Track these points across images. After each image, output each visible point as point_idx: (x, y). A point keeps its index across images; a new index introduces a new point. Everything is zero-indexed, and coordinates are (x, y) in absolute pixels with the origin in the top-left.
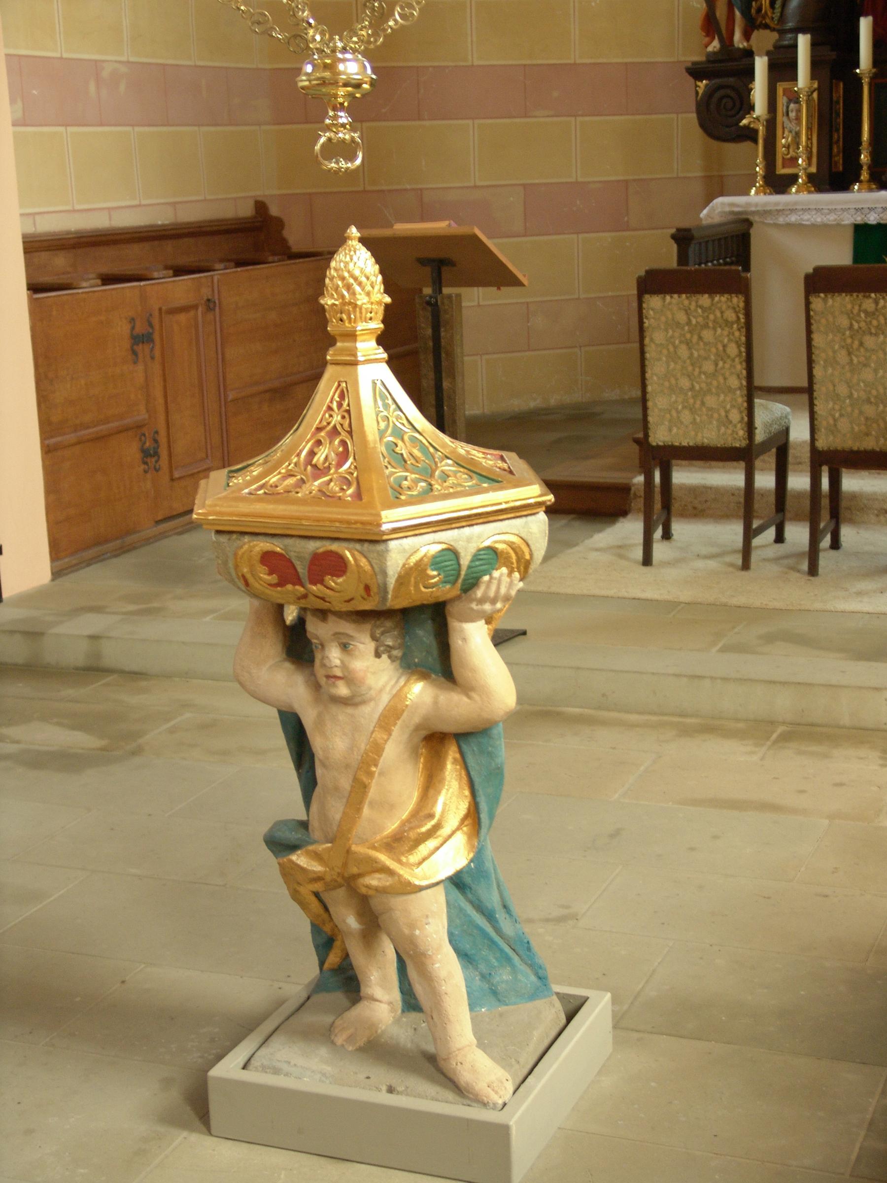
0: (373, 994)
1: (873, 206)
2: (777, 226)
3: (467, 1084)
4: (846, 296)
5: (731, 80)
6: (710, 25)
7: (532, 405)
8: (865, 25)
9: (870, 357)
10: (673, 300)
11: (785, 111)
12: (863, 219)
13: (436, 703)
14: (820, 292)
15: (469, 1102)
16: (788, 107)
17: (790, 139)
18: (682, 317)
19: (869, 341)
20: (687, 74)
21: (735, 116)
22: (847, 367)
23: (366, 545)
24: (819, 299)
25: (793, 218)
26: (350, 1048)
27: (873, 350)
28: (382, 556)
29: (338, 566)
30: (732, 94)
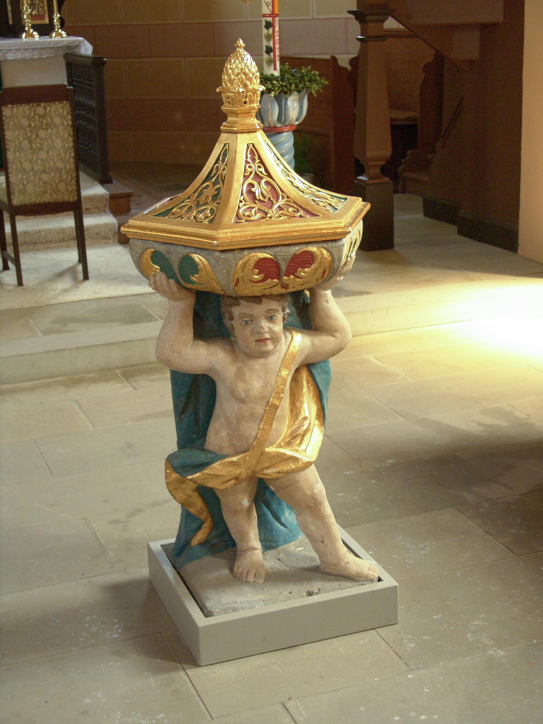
0: (254, 546)
3: (357, 573)
4: (26, 105)
9: (43, 143)
13: (313, 344)
14: (8, 104)
15: (362, 583)
19: (42, 134)
22: (29, 151)
23: (330, 244)
24: (8, 108)
26: (261, 582)
27: (45, 139)
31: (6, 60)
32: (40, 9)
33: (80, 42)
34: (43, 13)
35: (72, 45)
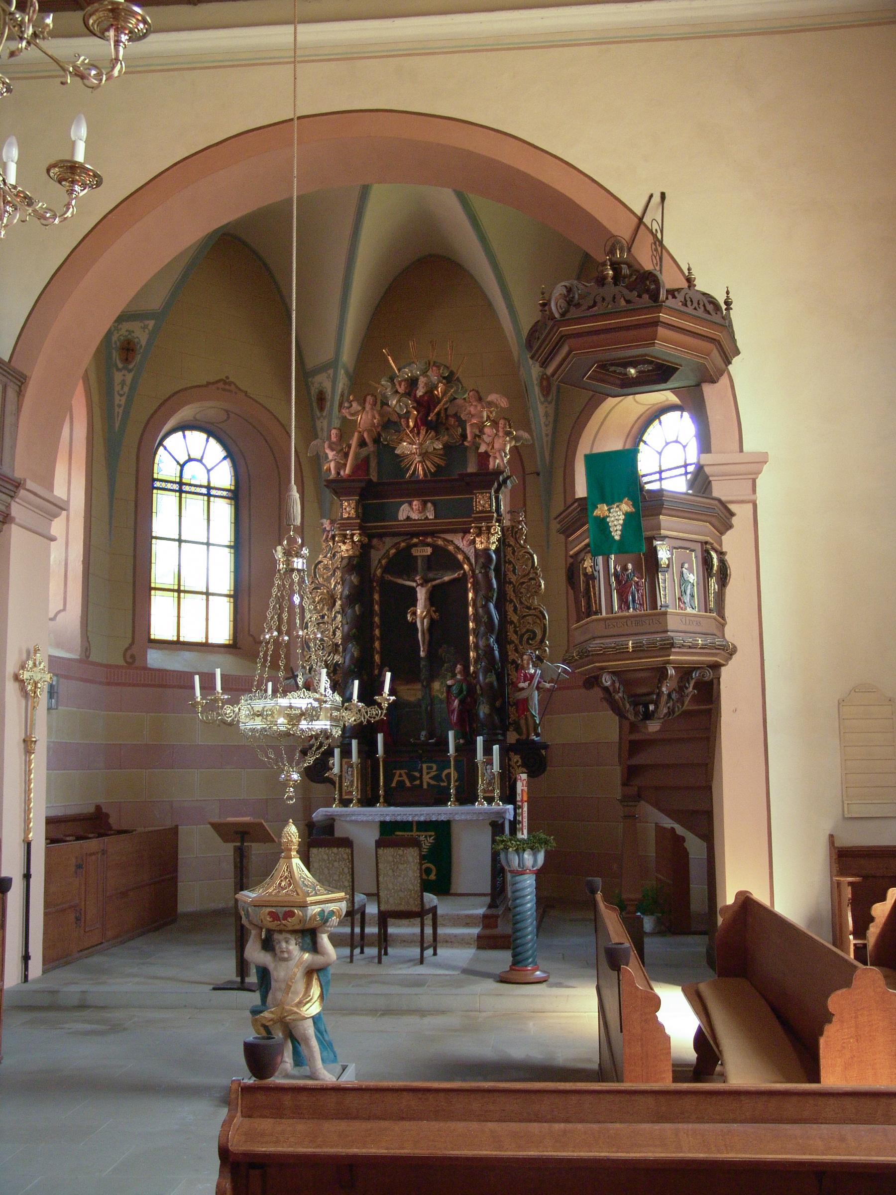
2: (346, 821)
7: (221, 906)
8: (380, 737)
10: (322, 850)
18: (326, 857)
19: (401, 867)
25: (353, 818)
28: (306, 911)
29: (292, 914)
31: (454, 820)
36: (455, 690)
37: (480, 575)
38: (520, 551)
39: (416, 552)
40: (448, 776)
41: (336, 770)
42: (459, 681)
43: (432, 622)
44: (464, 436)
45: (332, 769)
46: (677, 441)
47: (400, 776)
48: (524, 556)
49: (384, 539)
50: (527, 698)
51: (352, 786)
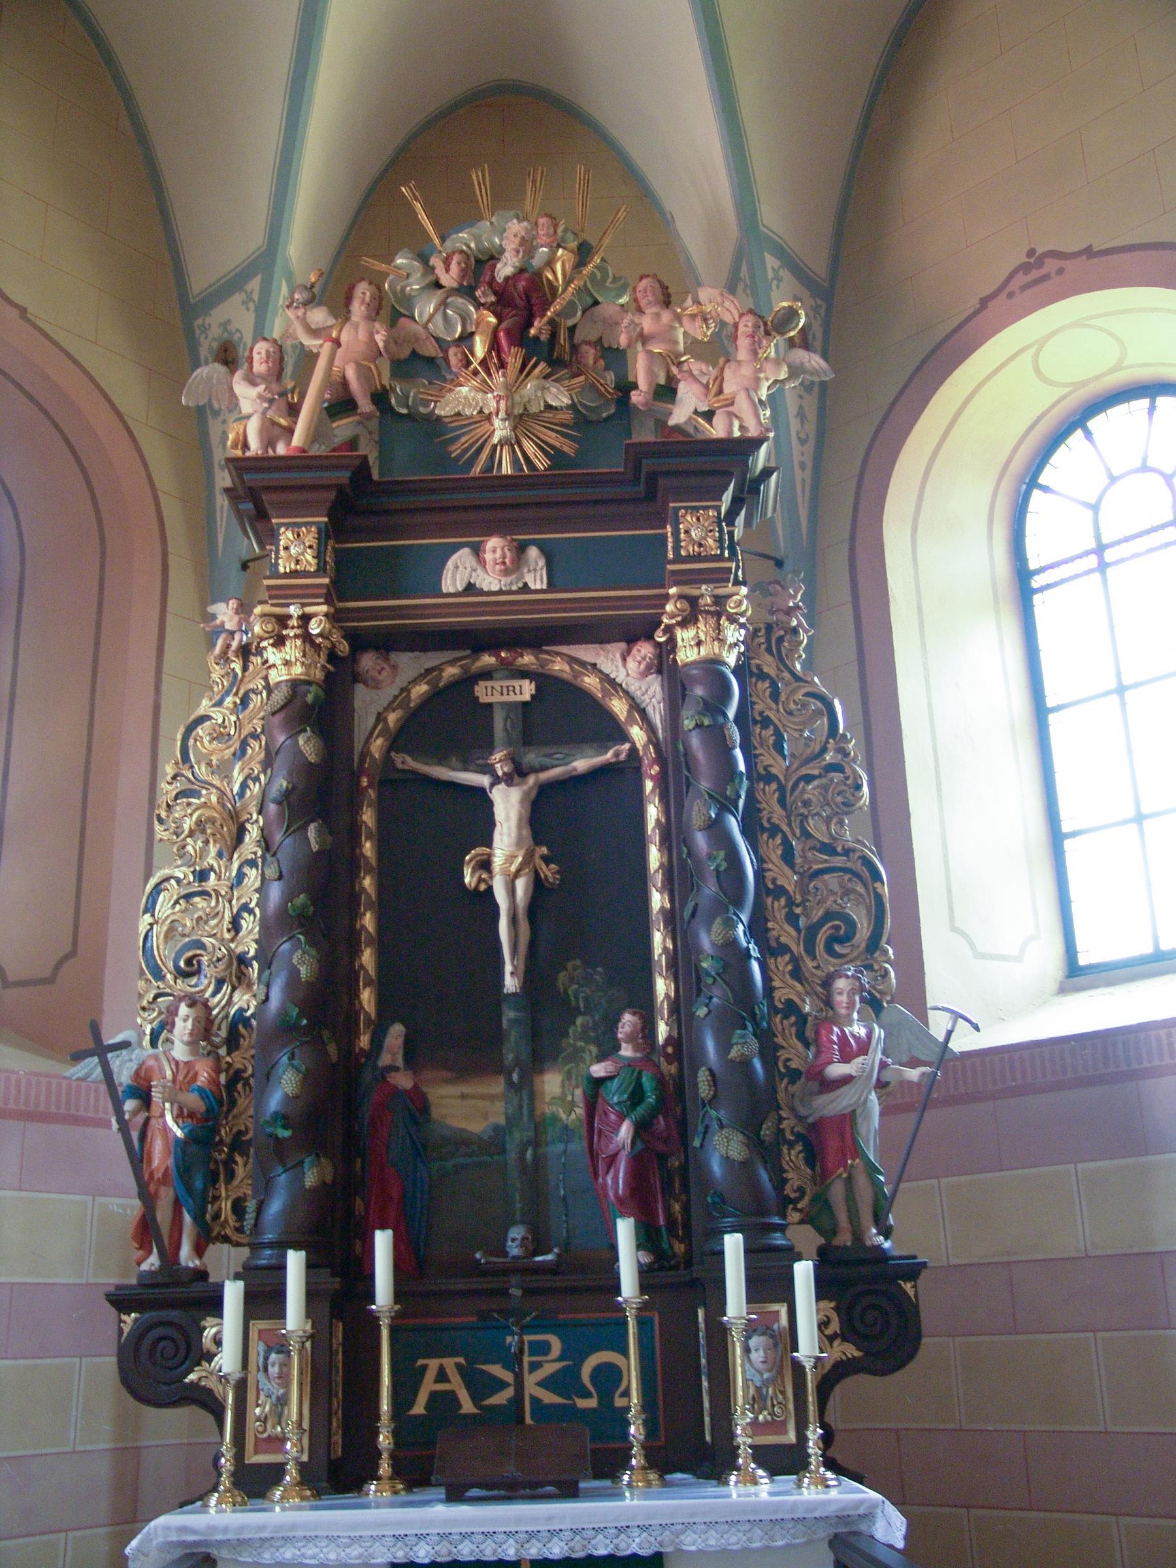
1: (424, 1532)
5: (174, 1314)
6: (146, 1232)
8: (383, 1241)
11: (261, 1364)
12: (407, 1554)
16: (266, 1358)
17: (267, 1408)
20: (108, 1305)
21: (177, 1368)
30: (177, 1336)
32: (776, 1409)
33: (874, 1505)
34: (782, 1419)
35: (850, 1513)
36: (614, 1095)
37: (695, 741)
38: (793, 692)
39: (485, 692)
40: (609, 1377)
41: (227, 1360)
42: (630, 1064)
43: (538, 885)
44: (626, 387)
45: (209, 1357)
46: (1144, 468)
47: (442, 1376)
48: (804, 705)
49: (394, 656)
50: (854, 1111)
51: (279, 1418)
